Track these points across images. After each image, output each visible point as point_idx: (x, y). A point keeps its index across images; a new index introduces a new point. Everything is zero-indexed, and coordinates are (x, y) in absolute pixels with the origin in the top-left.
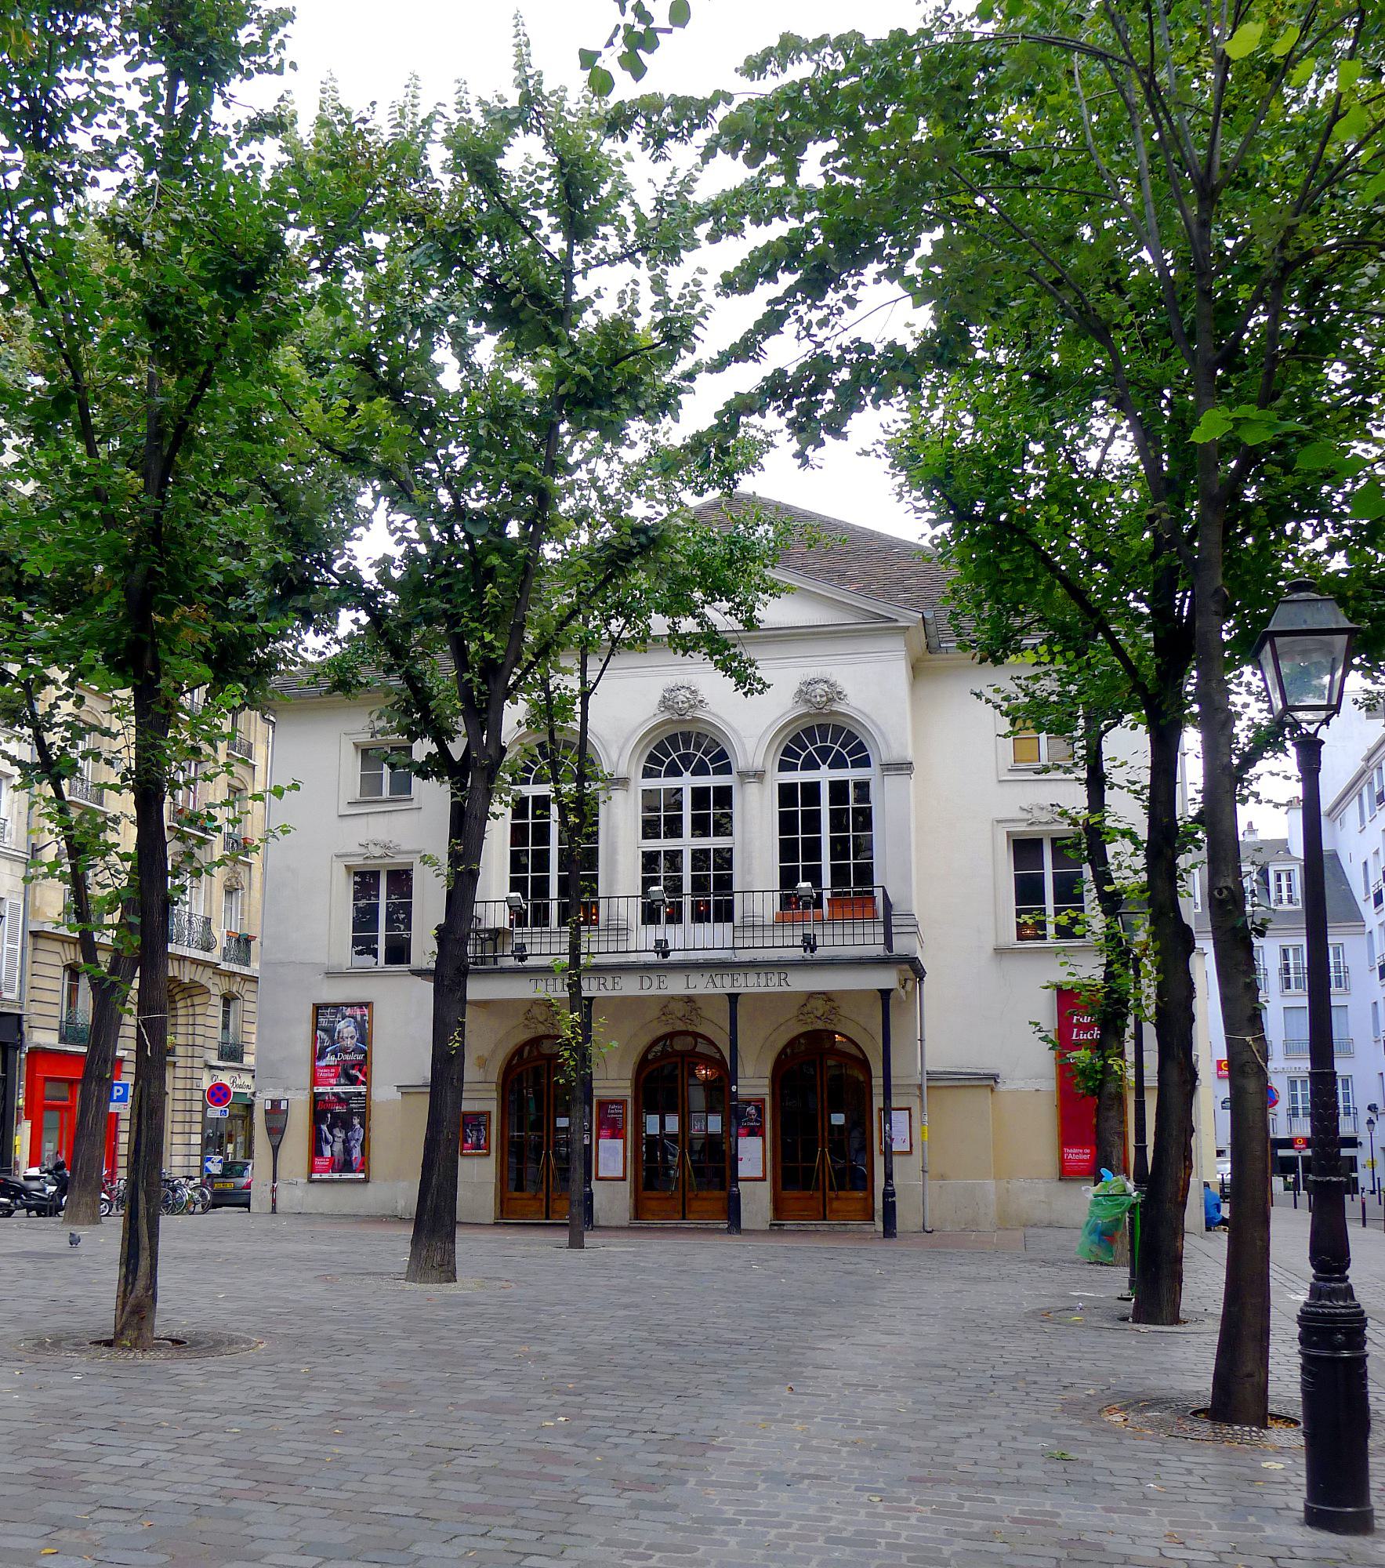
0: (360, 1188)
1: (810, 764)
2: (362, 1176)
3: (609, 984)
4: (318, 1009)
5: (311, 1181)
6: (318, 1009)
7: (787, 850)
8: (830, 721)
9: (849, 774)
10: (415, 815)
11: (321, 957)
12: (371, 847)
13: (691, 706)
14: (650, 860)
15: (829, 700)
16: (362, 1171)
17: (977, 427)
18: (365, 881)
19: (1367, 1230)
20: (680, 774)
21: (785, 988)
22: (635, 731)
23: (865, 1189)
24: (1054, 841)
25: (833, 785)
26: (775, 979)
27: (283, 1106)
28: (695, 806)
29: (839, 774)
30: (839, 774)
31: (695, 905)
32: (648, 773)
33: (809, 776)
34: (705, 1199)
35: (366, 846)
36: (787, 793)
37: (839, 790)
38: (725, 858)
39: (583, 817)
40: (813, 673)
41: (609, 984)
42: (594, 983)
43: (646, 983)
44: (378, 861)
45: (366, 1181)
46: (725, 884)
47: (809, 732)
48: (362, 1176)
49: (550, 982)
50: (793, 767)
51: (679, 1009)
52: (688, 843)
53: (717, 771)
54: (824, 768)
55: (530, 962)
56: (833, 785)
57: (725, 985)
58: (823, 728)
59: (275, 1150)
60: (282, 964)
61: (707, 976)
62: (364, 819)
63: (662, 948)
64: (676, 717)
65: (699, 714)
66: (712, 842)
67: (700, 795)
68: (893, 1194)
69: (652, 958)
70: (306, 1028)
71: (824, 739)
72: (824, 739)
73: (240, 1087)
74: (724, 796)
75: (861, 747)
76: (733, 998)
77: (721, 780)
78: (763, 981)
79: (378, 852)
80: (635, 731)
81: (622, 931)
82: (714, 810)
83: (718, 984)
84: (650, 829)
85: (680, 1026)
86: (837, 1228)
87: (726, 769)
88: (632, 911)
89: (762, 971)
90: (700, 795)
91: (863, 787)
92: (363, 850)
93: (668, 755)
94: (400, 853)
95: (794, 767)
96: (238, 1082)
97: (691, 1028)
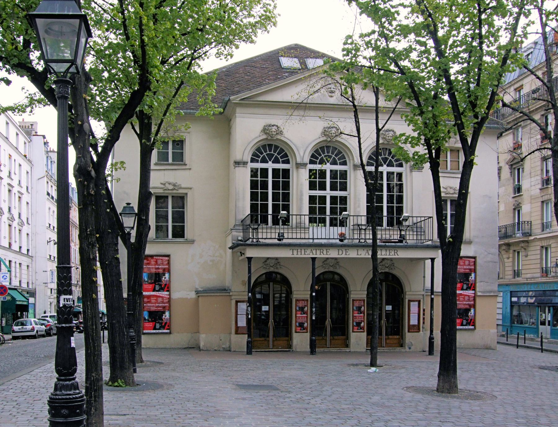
0: (166, 337)
1: (264, 161)
2: (168, 331)
3: (325, 252)
7: (254, 196)
8: (274, 143)
10: (188, 171)
12: (167, 185)
13: (277, 134)
14: (312, 199)
15: (277, 134)
16: (169, 329)
19: (518, 349)
20: (267, 162)
21: (396, 256)
22: (311, 143)
23: (398, 334)
25: (274, 170)
26: (393, 253)
28: (331, 178)
29: (391, 169)
30: (391, 169)
31: (331, 220)
32: (253, 161)
33: (264, 166)
34: (336, 339)
35: (164, 184)
36: (254, 173)
38: (344, 200)
39: (283, 179)
40: (273, 122)
41: (325, 252)
42: (384, 252)
43: (295, 252)
44: (170, 192)
45: (170, 333)
47: (264, 147)
48: (168, 331)
49: (299, 250)
50: (315, 163)
51: (332, 263)
52: (328, 193)
53: (284, 162)
54: (270, 163)
55: (285, 241)
56: (274, 170)
57: (309, 254)
58: (270, 146)
61: (365, 251)
62: (163, 172)
64: (269, 138)
65: (279, 137)
66: (339, 193)
67: (334, 174)
68: (433, 339)
71: (270, 151)
72: (270, 151)
75: (286, 155)
76: (314, 259)
77: (343, 168)
78: (388, 253)
79: (171, 187)
80: (311, 143)
81: (299, 226)
82: (340, 181)
83: (314, 253)
84: (312, 186)
85: (331, 269)
86: (392, 350)
87: (288, 162)
89: (388, 249)
90: (334, 174)
91: (400, 175)
92: (162, 186)
93: (262, 153)
94: (181, 188)
95: (257, 161)
97: (276, 270)
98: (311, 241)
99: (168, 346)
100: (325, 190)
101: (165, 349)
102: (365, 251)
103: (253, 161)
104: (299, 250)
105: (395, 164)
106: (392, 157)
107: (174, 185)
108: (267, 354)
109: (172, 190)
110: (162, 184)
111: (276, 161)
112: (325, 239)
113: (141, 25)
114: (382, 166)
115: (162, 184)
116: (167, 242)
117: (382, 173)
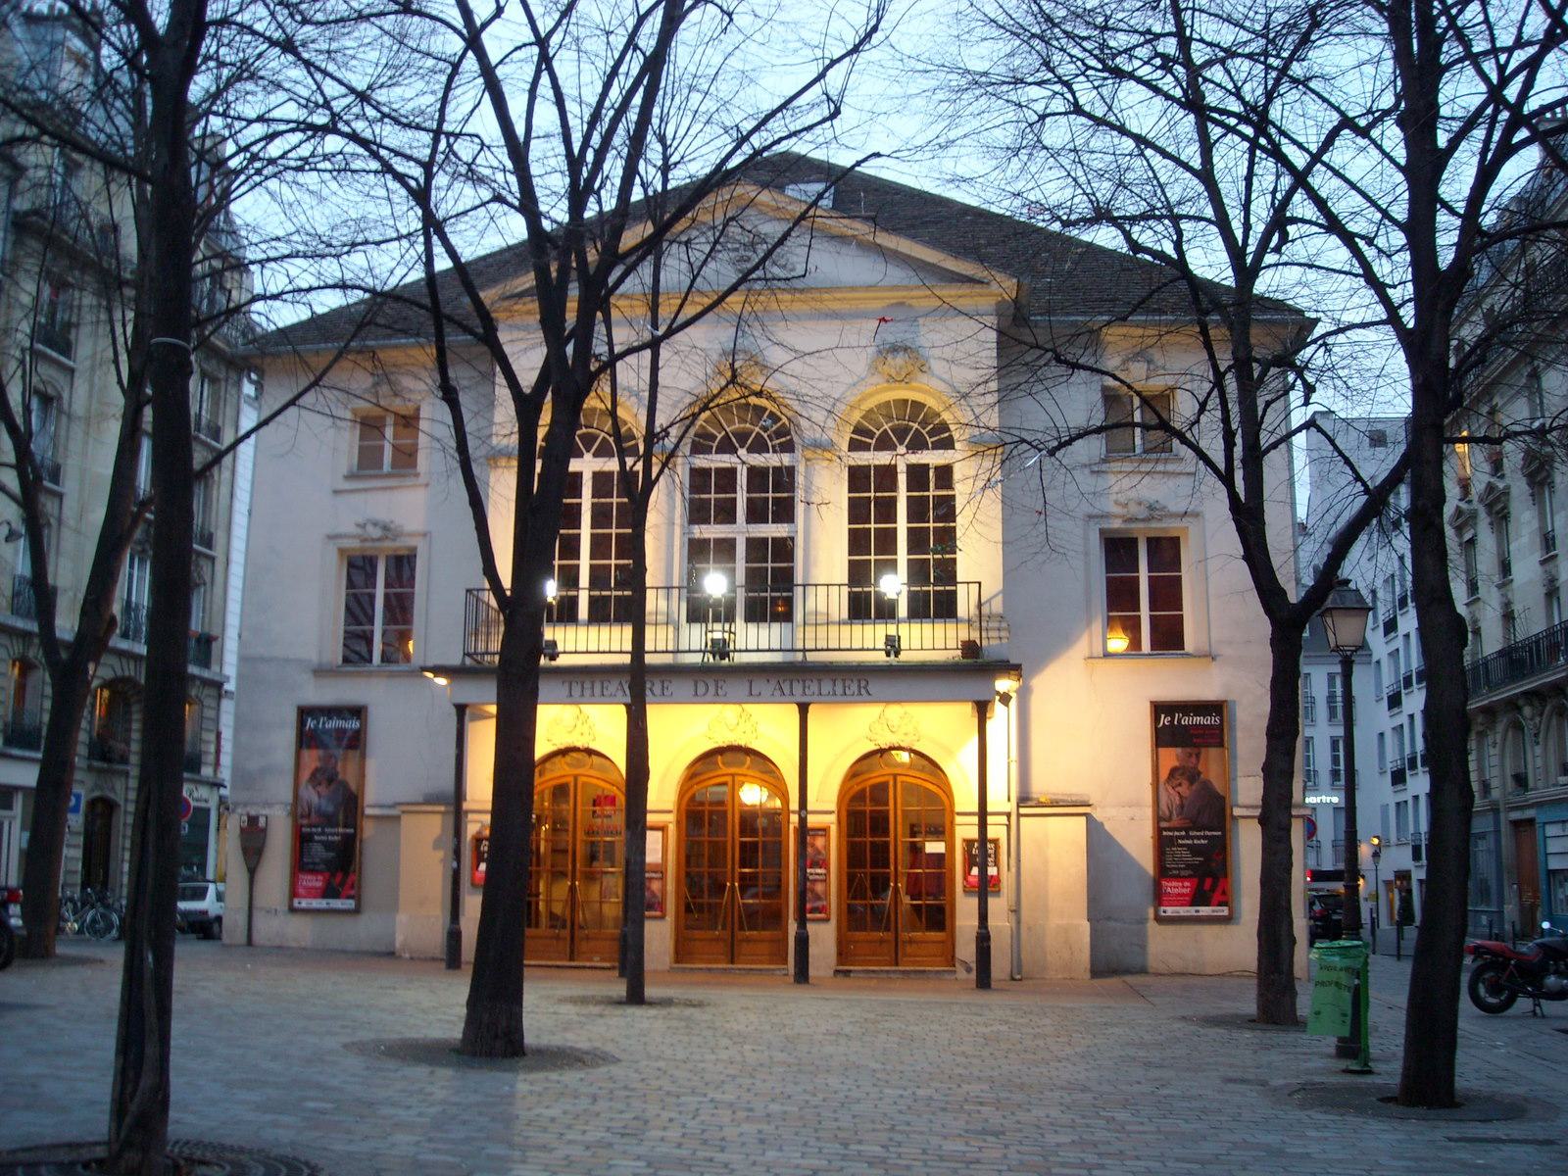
4: (304, 712)
5: (292, 910)
6: (304, 712)
9: (932, 458)
11: (312, 655)
12: (370, 528)
17: (135, 148)
18: (359, 567)
20: (894, 448)
24: (1149, 540)
27: (262, 822)
29: (758, 460)
30: (758, 460)
32: (855, 446)
33: (883, 458)
35: (363, 526)
36: (858, 478)
37: (917, 475)
38: (784, 549)
44: (377, 544)
45: (357, 911)
46: (785, 579)
48: (658, 913)
49: (587, 685)
50: (866, 447)
53: (937, 446)
54: (588, 456)
59: (252, 872)
60: (262, 659)
61: (773, 682)
63: (721, 649)
66: (772, 530)
67: (757, 476)
69: (880, 657)
70: (288, 736)
73: (197, 800)
74: (785, 478)
75: (783, 432)
79: (376, 533)
87: (788, 447)
88: (838, 603)
91: (945, 474)
92: (359, 531)
96: (195, 795)
98: (799, 656)
99: (351, 947)
100: (750, 542)
101: (426, 960)
102: (773, 682)
103: (855, 446)
104: (587, 685)
105: (930, 441)
106: (924, 423)
107: (385, 528)
108: (569, 973)
109: (379, 540)
110: (358, 525)
111: (759, 447)
112: (769, 650)
113: (364, 143)
114: (580, 455)
115: (358, 525)
116: (370, 674)
117: (579, 475)
